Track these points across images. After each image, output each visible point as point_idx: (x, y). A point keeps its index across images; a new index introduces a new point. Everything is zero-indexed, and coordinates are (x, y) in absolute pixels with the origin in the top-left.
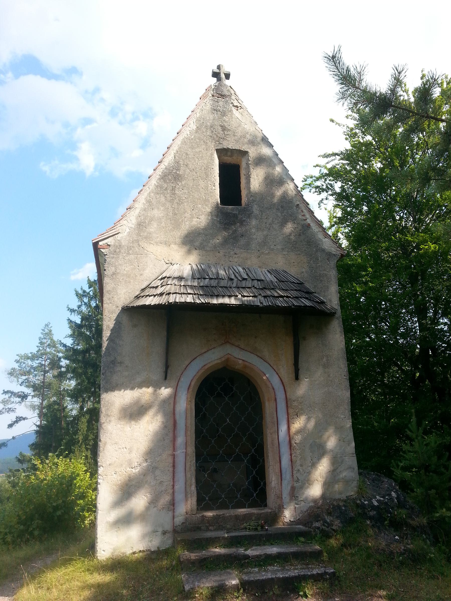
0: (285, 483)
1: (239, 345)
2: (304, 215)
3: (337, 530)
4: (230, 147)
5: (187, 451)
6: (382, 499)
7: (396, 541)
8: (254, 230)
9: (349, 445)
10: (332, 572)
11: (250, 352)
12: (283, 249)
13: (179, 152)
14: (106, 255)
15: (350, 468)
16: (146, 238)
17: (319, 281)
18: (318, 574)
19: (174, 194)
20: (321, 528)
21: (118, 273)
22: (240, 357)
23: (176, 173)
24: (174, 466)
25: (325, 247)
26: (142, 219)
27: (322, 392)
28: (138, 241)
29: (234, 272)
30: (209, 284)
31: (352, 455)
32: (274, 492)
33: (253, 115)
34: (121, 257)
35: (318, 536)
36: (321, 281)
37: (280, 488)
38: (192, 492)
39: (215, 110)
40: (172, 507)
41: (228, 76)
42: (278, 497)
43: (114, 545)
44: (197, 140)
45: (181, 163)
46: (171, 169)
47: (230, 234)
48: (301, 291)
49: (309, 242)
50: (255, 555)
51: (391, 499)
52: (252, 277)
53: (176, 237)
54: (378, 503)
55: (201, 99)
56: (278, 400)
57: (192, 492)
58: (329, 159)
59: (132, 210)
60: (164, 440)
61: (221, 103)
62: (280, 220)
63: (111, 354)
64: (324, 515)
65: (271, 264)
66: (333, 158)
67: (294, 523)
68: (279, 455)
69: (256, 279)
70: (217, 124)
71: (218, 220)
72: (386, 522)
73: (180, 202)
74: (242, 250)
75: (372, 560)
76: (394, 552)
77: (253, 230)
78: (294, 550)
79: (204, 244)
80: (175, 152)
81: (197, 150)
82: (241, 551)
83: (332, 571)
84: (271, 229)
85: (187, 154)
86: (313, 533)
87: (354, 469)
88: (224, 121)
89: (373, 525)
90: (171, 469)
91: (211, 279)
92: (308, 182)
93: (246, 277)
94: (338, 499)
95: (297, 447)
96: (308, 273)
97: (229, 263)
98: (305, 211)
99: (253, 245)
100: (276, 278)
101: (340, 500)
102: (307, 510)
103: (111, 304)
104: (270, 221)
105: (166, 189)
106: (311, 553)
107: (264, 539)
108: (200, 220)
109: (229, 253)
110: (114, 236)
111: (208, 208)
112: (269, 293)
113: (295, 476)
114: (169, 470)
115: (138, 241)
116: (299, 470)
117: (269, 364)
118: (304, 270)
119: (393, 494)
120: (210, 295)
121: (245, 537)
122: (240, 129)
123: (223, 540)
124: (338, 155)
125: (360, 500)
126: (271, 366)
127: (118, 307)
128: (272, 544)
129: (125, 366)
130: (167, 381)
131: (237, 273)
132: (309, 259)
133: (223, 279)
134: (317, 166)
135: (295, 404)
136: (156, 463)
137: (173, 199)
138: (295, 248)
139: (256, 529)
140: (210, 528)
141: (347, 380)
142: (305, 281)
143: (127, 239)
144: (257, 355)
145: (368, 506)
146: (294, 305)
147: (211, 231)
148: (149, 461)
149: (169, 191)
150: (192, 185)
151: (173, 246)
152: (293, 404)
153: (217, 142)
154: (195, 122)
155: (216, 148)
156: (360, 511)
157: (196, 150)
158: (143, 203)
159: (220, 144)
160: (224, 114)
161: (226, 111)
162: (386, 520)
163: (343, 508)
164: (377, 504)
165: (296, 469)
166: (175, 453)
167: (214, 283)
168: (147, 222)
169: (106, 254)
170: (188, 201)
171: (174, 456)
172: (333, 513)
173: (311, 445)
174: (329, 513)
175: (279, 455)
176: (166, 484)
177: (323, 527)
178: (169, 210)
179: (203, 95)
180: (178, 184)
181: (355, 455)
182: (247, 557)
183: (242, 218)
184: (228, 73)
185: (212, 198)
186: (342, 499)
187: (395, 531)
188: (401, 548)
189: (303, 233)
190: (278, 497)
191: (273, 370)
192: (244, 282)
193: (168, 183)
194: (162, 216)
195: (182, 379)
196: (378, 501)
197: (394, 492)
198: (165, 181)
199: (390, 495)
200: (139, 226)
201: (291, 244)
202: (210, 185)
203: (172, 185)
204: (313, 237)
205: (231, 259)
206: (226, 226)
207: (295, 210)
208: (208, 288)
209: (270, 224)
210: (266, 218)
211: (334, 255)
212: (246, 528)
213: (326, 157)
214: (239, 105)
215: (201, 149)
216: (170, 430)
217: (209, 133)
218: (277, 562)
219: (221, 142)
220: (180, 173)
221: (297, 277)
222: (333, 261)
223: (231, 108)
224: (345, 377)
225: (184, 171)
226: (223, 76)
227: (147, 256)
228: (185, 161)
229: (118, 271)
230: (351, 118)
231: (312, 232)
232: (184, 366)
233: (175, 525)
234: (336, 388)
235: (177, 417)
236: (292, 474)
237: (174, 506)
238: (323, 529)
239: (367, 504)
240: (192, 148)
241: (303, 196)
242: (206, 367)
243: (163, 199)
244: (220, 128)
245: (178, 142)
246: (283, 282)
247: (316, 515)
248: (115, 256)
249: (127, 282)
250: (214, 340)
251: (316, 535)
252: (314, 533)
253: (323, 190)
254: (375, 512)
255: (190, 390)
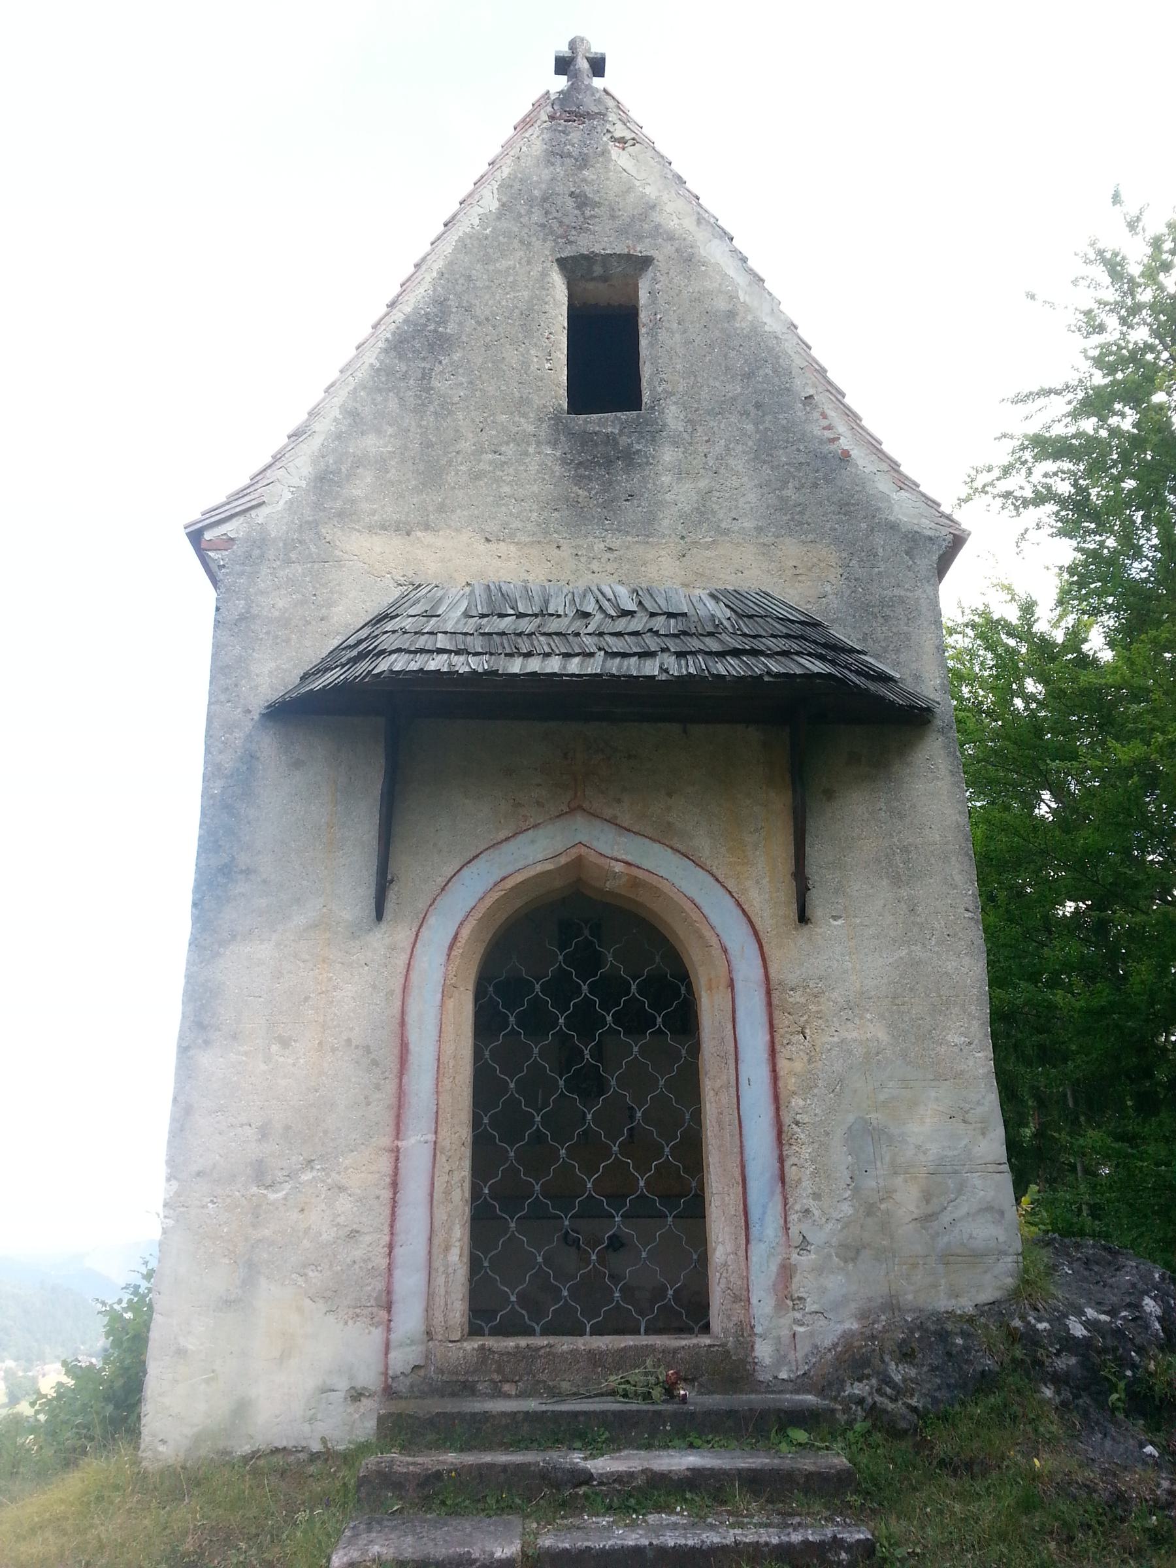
0: (758, 1251)
1: (616, 817)
2: (829, 428)
3: (928, 1411)
4: (597, 249)
5: (439, 1140)
6: (1103, 1317)
7: (1145, 1463)
8: (669, 478)
9: (983, 1134)
10: (859, 1541)
11: (650, 838)
12: (759, 529)
13: (446, 276)
14: (224, 566)
15: (989, 1209)
16: (339, 516)
17: (881, 620)
18: (806, 1542)
19: (428, 390)
20: (870, 1400)
21: (254, 617)
22: (616, 854)
23: (436, 331)
24: (395, 1185)
25: (900, 516)
26: (331, 461)
27: (891, 960)
28: (314, 525)
29: (600, 597)
30: (513, 627)
31: (991, 1168)
32: (723, 1281)
33: (671, 159)
34: (264, 570)
35: (858, 1426)
36: (886, 618)
37: (743, 1266)
38: (450, 1270)
39: (555, 154)
40: (383, 1314)
41: (598, 66)
42: (737, 1299)
43: (198, 1425)
44: (501, 238)
45: (453, 302)
46: (423, 321)
47: (593, 492)
48: (806, 640)
49: (848, 504)
50: (612, 1473)
51: (1140, 1320)
52: (653, 608)
53: (430, 508)
54: (1089, 1331)
55: (518, 129)
56: (739, 986)
57: (450, 1270)
58: (1030, 407)
59: (300, 439)
60: (368, 1104)
61: (575, 136)
62: (750, 443)
63: (220, 846)
64: (887, 1358)
65: (722, 576)
66: (1042, 401)
67: (790, 1386)
68: (742, 1160)
69: (665, 613)
70: (561, 192)
71: (558, 454)
72: (1115, 1396)
73: (446, 409)
74: (629, 538)
75: (1038, 1518)
76: (1131, 1498)
77: (666, 479)
78: (753, 1466)
79: (513, 526)
80: (435, 274)
81: (502, 264)
82: (576, 1458)
83: (862, 1536)
84: (722, 471)
85: (469, 278)
86: (842, 1418)
87: (1002, 1213)
88: (584, 180)
89: (1064, 1404)
90: (386, 1194)
91: (520, 616)
92: (978, 484)
93: (632, 606)
94: (947, 1312)
95: (802, 1136)
96: (842, 597)
97: (591, 576)
98: (831, 413)
99: (666, 522)
100: (732, 609)
101: (951, 1314)
102: (835, 1346)
103: (230, 704)
104: (719, 448)
105: (405, 377)
106: (809, 1476)
107: (668, 1428)
108: (503, 458)
109: (590, 547)
110: (248, 515)
111: (528, 423)
112: (694, 644)
113: (794, 1231)
114: (378, 1198)
115: (314, 525)
116: (807, 1211)
117: (713, 875)
118: (828, 588)
119: (1150, 1305)
120: (506, 655)
121: (602, 1417)
122: (631, 198)
123: (526, 1425)
124: (1056, 394)
125: (1023, 1318)
126: (717, 880)
127: (249, 711)
128: (691, 1446)
129: (259, 880)
130: (384, 925)
131: (609, 600)
132: (844, 555)
133: (559, 616)
134: (1004, 436)
135: (797, 997)
136: (339, 1173)
137: (423, 405)
138: (800, 524)
139: (647, 1397)
140: (506, 1387)
141: (977, 922)
142: (833, 621)
143: (285, 520)
144: (671, 848)
145: (1049, 1336)
146: (769, 673)
147: (535, 488)
148: (319, 1167)
149: (412, 382)
150: (480, 361)
151: (419, 534)
152: (791, 1000)
153: (559, 240)
154: (495, 191)
155: (559, 256)
156: (1019, 1353)
157: (497, 265)
158: (335, 420)
159: (571, 243)
160: (583, 162)
161: (591, 155)
162: (1114, 1388)
163: (959, 1341)
164: (1085, 1332)
165: (797, 1207)
166: (400, 1144)
167: (526, 625)
168: (343, 470)
169: (222, 563)
170: (468, 407)
171: (396, 1154)
172: (920, 1355)
173: (850, 1128)
174: (905, 1355)
175: (742, 1160)
176: (368, 1239)
177: (878, 1398)
178: (410, 434)
179: (523, 120)
180: (440, 362)
181: (1006, 1167)
182: (585, 1478)
183: (630, 445)
184: (599, 56)
185: (542, 393)
186: (959, 1312)
187: (1148, 1429)
188: (1158, 1485)
189: (825, 479)
190: (737, 1299)
191: (722, 891)
192: (624, 620)
193: (409, 360)
194: (389, 452)
195: (432, 920)
196: (1089, 1324)
197: (1154, 1298)
198: (401, 356)
199: (1136, 1306)
200: (321, 481)
201: (785, 514)
202: (535, 360)
203: (423, 365)
204: (858, 488)
205: (595, 566)
206: (581, 471)
207: (799, 414)
208: (504, 637)
209: (720, 458)
210: (707, 441)
211: (930, 539)
212: (613, 1393)
213: (1022, 401)
214: (628, 135)
215: (512, 263)
216: (387, 1074)
217: (537, 216)
218: (686, 1500)
219: (572, 239)
220: (448, 331)
221: (807, 610)
222: (925, 558)
223: (606, 144)
224: (970, 915)
225: (460, 324)
226: (583, 65)
227: (342, 567)
228: (465, 298)
229: (255, 611)
230: (1087, 284)
231: (857, 475)
232: (441, 881)
233: (391, 1373)
234: (937, 949)
235: (413, 1037)
236: (786, 1221)
237: (389, 1312)
238: (875, 1403)
239: (1045, 1330)
240: (487, 260)
241: (826, 371)
242: (509, 883)
243: (393, 404)
244: (570, 202)
245: (448, 247)
246: (750, 617)
247: (858, 1357)
248: (248, 569)
249: (279, 641)
250: (538, 803)
251: (850, 1423)
252: (845, 1417)
253: (1026, 503)
254: (1073, 1361)
255: (457, 952)
